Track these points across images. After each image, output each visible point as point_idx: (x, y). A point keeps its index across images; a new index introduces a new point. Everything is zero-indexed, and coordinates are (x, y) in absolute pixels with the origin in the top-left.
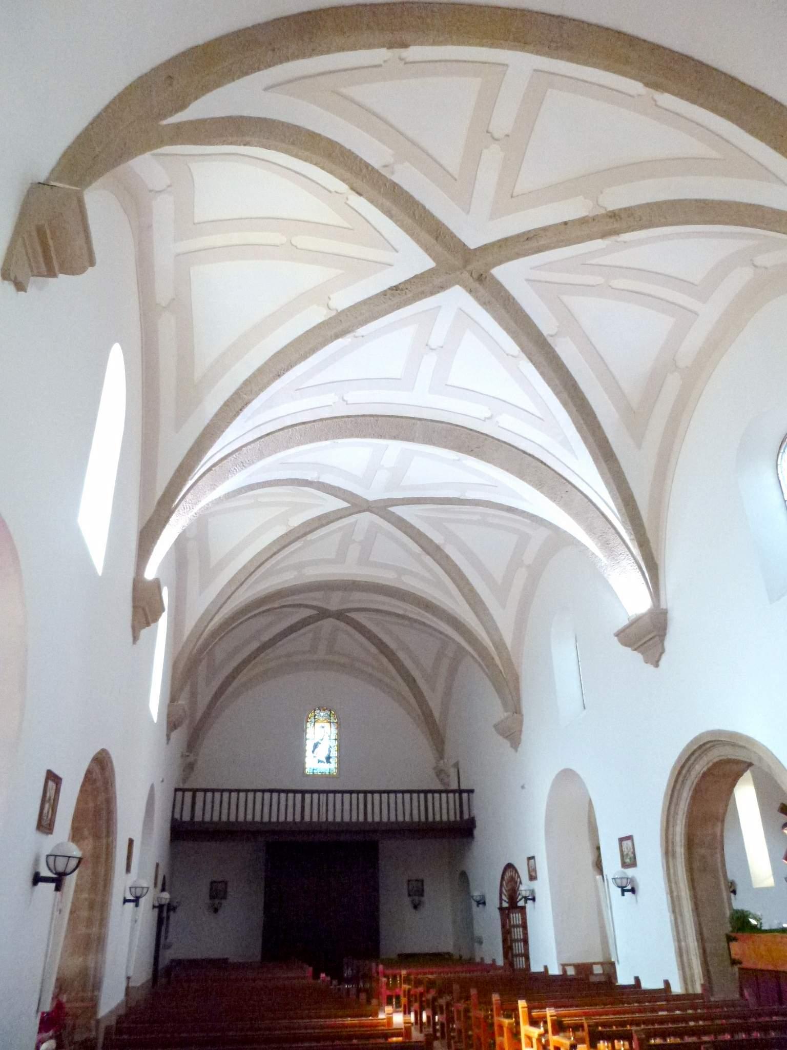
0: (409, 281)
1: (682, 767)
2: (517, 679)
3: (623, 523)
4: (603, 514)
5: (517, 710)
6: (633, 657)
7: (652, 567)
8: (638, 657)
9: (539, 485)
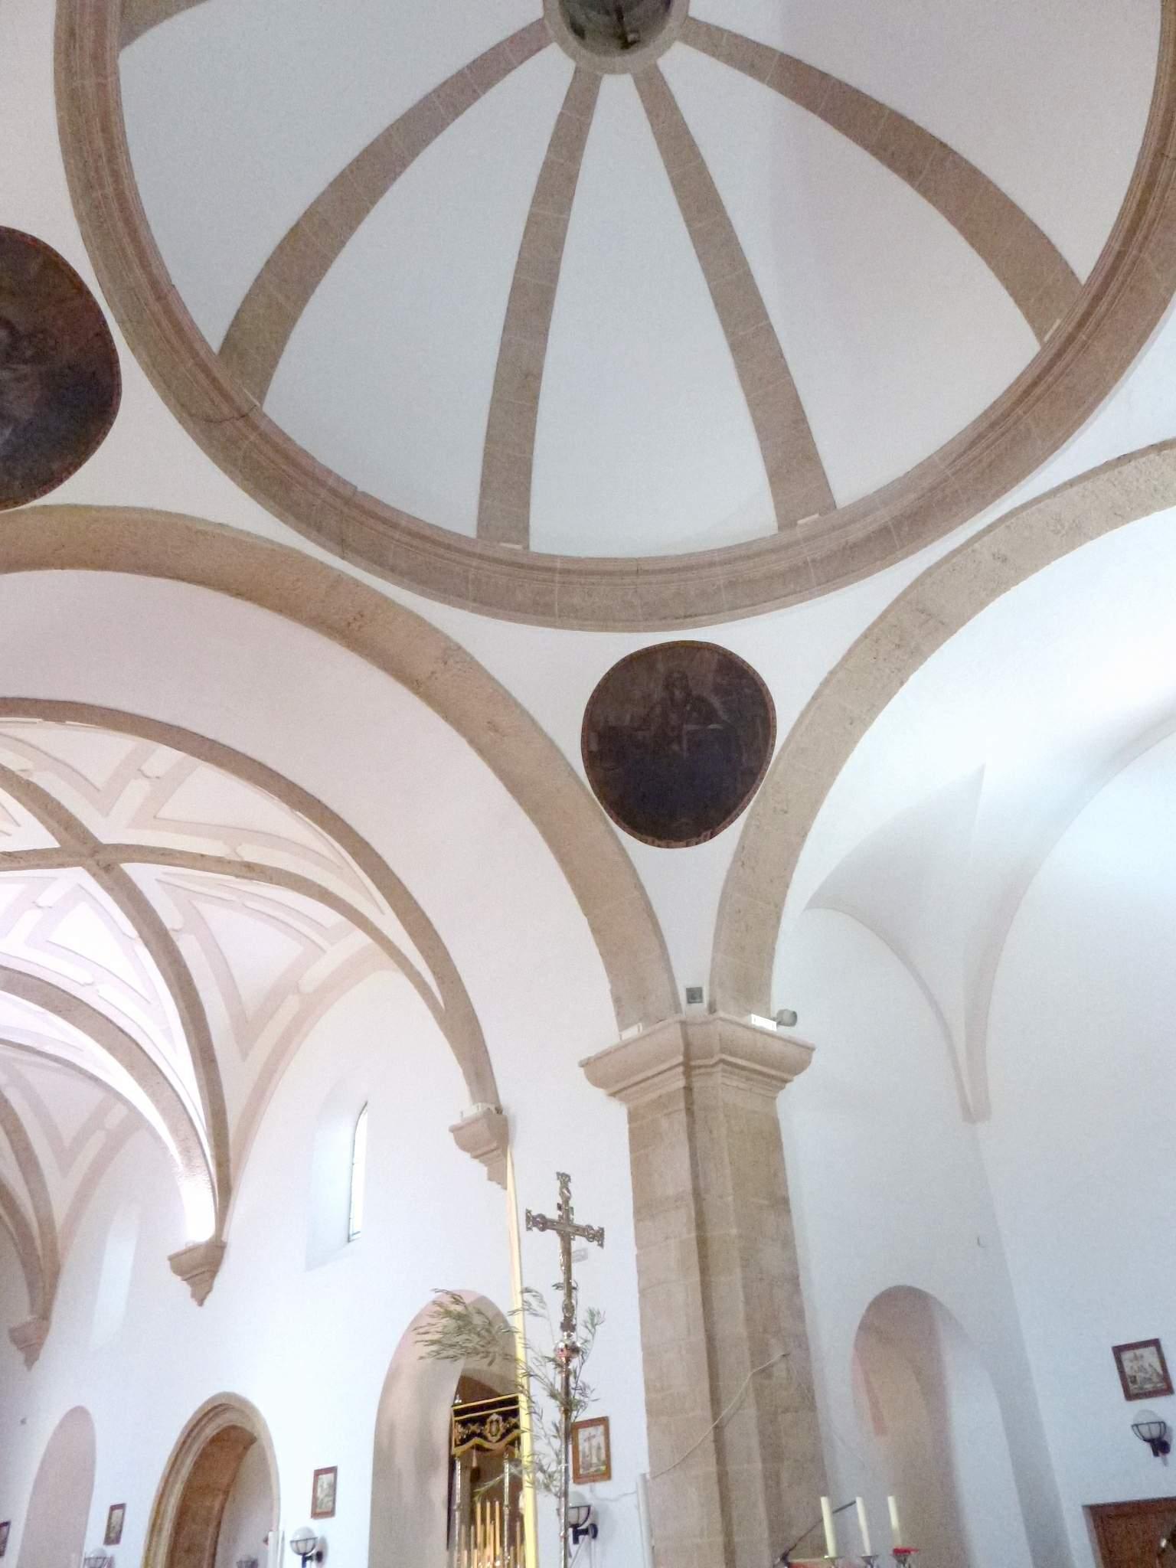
0: (27, 852)
1: (195, 1426)
2: (56, 1274)
3: (208, 1136)
4: (191, 1120)
5: (44, 1315)
6: (181, 1288)
7: (224, 1190)
8: (185, 1288)
9: (131, 1067)
